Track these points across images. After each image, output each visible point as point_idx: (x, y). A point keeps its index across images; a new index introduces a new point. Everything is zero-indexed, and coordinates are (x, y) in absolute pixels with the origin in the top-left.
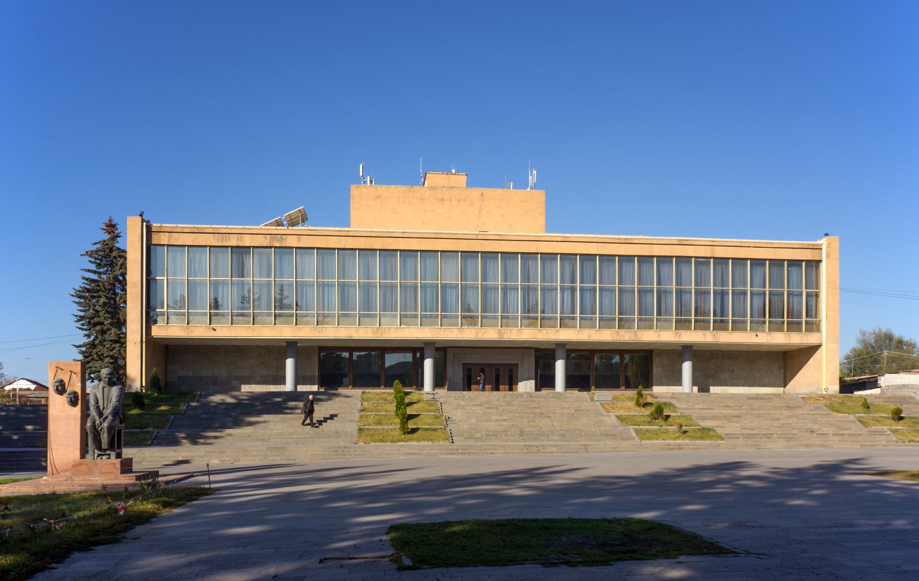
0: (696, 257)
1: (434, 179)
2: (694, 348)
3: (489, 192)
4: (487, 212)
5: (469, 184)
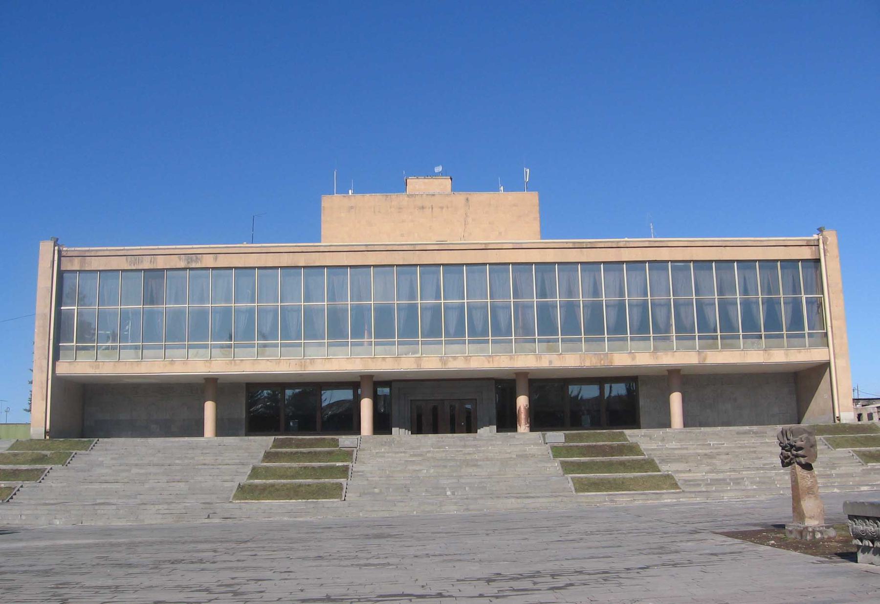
0: (672, 261)
1: (415, 184)
2: (682, 373)
3: (480, 198)
4: (473, 220)
5: (454, 189)
